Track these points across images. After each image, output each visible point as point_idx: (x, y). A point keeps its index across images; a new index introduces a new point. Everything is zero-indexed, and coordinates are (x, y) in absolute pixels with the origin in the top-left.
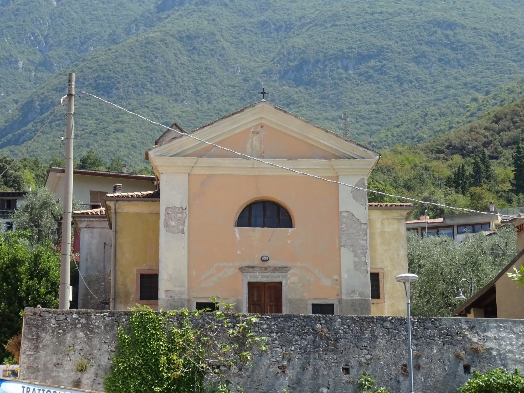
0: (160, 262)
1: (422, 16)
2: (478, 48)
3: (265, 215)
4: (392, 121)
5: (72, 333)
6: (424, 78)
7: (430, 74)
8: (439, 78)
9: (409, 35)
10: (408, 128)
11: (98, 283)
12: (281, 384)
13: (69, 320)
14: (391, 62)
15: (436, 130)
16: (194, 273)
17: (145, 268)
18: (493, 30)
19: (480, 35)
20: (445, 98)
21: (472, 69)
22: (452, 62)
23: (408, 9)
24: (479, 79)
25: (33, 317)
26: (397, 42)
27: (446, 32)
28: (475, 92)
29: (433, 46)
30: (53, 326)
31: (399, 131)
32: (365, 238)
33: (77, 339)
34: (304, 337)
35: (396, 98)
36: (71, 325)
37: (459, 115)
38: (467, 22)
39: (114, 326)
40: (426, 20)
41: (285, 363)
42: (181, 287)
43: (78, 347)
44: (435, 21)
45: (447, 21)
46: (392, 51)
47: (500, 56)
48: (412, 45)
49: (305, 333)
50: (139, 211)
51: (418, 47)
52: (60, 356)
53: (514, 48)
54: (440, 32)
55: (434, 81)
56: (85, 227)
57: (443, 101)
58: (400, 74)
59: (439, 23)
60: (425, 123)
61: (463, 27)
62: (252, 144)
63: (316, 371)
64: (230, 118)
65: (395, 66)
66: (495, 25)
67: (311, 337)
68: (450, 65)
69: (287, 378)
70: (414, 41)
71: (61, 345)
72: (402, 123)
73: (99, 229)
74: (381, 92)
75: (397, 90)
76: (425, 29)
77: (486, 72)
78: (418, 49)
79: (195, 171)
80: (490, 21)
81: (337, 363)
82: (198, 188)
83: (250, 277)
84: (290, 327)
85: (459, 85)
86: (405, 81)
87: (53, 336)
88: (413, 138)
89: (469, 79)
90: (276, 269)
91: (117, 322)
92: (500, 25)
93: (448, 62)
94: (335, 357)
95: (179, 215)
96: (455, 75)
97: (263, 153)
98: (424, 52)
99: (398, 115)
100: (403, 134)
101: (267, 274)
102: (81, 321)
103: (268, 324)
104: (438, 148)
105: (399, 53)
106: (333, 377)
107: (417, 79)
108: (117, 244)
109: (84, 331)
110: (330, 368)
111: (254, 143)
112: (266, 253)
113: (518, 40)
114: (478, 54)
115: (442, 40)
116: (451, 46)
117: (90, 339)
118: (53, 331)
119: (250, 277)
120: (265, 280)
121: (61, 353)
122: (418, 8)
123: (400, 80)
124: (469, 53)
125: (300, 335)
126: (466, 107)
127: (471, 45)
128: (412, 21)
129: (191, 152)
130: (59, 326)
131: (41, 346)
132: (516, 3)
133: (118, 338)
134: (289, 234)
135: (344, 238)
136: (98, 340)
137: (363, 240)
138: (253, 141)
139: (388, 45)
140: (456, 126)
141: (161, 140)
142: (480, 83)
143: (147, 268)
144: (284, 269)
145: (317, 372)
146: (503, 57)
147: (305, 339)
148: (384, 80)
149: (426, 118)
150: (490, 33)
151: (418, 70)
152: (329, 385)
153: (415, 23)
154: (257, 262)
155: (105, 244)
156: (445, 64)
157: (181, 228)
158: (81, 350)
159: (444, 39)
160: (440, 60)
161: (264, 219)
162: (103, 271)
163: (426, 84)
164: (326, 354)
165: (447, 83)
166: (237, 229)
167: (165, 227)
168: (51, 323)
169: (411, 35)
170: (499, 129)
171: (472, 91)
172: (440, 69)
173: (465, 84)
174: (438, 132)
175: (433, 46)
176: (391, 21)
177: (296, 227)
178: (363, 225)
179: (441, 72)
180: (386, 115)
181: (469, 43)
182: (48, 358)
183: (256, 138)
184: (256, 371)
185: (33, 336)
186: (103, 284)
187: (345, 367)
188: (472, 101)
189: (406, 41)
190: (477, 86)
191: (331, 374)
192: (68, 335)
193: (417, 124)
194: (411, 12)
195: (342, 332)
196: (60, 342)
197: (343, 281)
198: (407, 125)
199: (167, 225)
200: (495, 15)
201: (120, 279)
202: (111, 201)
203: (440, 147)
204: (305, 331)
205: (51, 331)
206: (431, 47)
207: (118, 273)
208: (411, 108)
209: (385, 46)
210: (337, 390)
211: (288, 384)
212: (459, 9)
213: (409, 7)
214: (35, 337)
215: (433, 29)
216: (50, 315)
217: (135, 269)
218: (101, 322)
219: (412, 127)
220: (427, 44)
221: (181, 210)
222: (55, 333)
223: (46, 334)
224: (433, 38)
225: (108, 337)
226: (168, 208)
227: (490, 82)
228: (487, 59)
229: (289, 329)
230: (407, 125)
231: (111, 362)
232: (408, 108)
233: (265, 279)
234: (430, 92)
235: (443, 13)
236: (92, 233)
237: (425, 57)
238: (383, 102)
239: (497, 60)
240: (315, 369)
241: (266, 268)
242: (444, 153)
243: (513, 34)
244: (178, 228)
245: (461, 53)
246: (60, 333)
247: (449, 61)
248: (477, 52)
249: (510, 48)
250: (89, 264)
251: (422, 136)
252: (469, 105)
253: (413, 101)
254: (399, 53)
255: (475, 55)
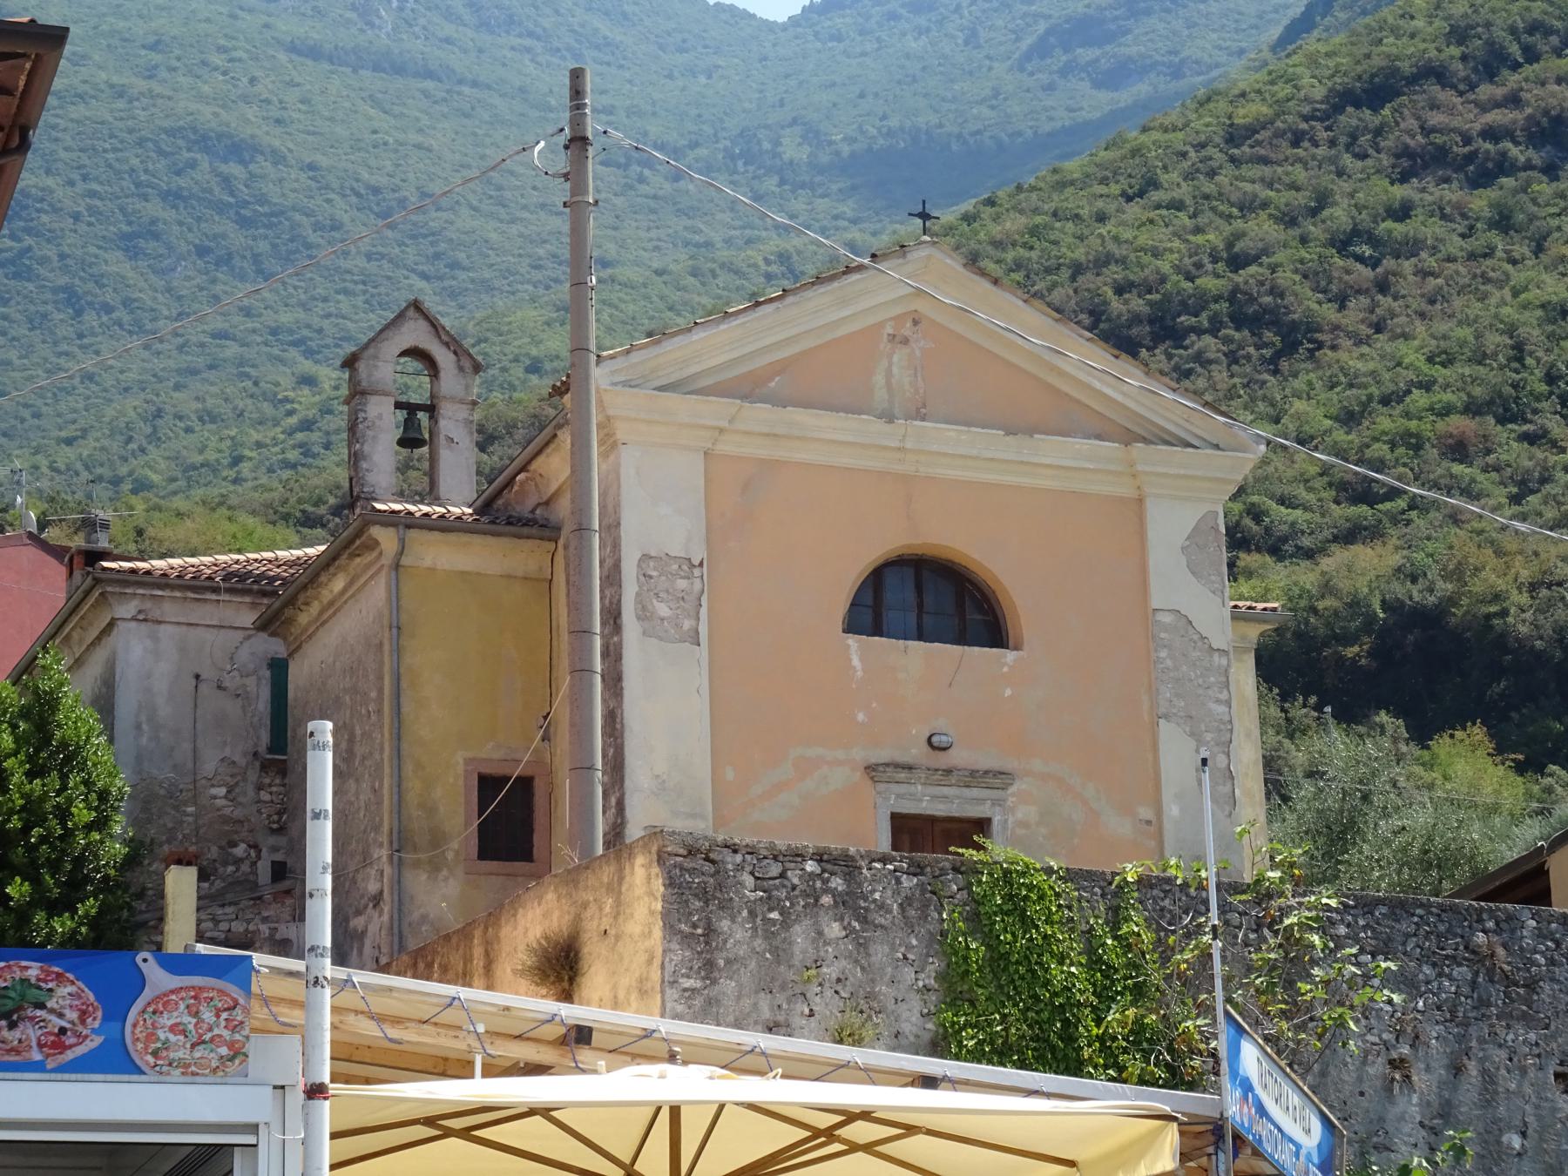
0: (627, 734)
1: (153, 110)
2: (317, 227)
3: (920, 606)
4: (43, 422)
5: (807, 922)
6: (149, 303)
7: (169, 290)
8: (196, 306)
9: (110, 166)
10: (103, 449)
11: (176, 808)
12: (1402, 1118)
13: (796, 881)
14: (48, 241)
15: (189, 461)
16: (730, 774)
17: (508, 751)
18: (365, 175)
19: (327, 187)
20: (211, 367)
21: (295, 288)
22: (237, 262)
23: (112, 86)
24: (316, 320)
25: (688, 864)
26: (71, 183)
27: (223, 168)
28: (301, 359)
29: (182, 205)
30: (752, 896)
31: (73, 457)
32: (1224, 696)
33: (826, 943)
34: (1446, 970)
35: (60, 354)
36: (805, 895)
37: (260, 423)
38: (291, 146)
39: (928, 906)
40: (166, 124)
41: (1405, 1050)
42: (693, 816)
43: (830, 971)
44: (195, 130)
45: (231, 136)
46: (56, 210)
47: (383, 256)
48: (118, 198)
49: (1447, 957)
50: (461, 567)
51: (138, 206)
52: (781, 998)
53: (425, 236)
54: (206, 165)
55: (180, 314)
56: (134, 619)
57: (205, 375)
58: (77, 281)
59: (205, 138)
60: (154, 437)
61: (278, 158)
62: (889, 374)
63: (1488, 1078)
64: (836, 284)
65: (62, 256)
66: (373, 162)
67: (1461, 972)
68: (232, 269)
69: (1415, 1099)
70: (124, 183)
71: (779, 963)
72: (85, 432)
73: (177, 629)
74: (13, 333)
75: (61, 332)
76: (161, 152)
77: (338, 302)
78: (134, 212)
79: (727, 446)
80: (359, 150)
81: (1539, 1056)
82: (738, 496)
83: (898, 796)
84: (1408, 936)
85: (254, 331)
86: (90, 304)
87: (754, 929)
88: (116, 482)
89: (286, 318)
90: (976, 777)
91: (933, 893)
92: (388, 163)
93: (226, 260)
94: (1532, 1036)
95: (682, 584)
96: (246, 302)
97: (924, 406)
98: (154, 222)
99: (62, 407)
100: (87, 468)
101: (946, 790)
102: (832, 885)
103: (1348, 926)
104: (303, 511)
105: (76, 217)
106: (1534, 1099)
107: (127, 302)
108: (402, 671)
109: (842, 919)
110: (1523, 1071)
111: (895, 370)
112: (940, 724)
113: (439, 214)
114: (318, 246)
115: (210, 191)
116: (237, 213)
117: (862, 945)
118: (752, 914)
119: (898, 796)
120: (940, 810)
121: (783, 988)
122: (142, 84)
123: (73, 301)
124: (292, 240)
125: (1434, 965)
126: (281, 401)
127: (297, 217)
128: (120, 124)
129: (709, 381)
130: (769, 898)
131: (721, 963)
132: (435, 102)
133: (941, 941)
134: (1005, 669)
135: (1166, 693)
136: (886, 949)
137: (1218, 701)
138: (890, 365)
139: (43, 190)
140: (253, 454)
141: (371, 351)
142: (320, 331)
143: (497, 755)
144: (997, 778)
145: (1493, 1082)
146: (391, 261)
147: (1450, 978)
148: (26, 297)
149: (159, 422)
150: (355, 185)
151: (131, 274)
152: (1525, 1124)
153: (131, 131)
154: (916, 752)
155: (197, 677)
156: (217, 264)
157: (687, 624)
158: (839, 980)
159: (217, 190)
160: (202, 251)
161: (919, 616)
162: (190, 765)
163: (154, 320)
164: (1508, 1027)
165: (219, 324)
166: (853, 641)
167: (638, 618)
168: (741, 884)
169: (117, 165)
170: (492, 469)
171: (293, 353)
172: (200, 280)
173: (274, 332)
174: (195, 468)
175: (182, 205)
176: (57, 116)
177: (1026, 646)
178: (1216, 656)
179: (201, 289)
180: (26, 406)
181: (294, 209)
182: (747, 1003)
183: (899, 356)
184: (1333, 1072)
185: (695, 926)
186: (190, 809)
187: (1560, 1069)
188: (299, 383)
189: (101, 183)
190: (311, 339)
191: (1528, 1090)
192: (797, 928)
193: (130, 439)
194: (121, 95)
195: (1543, 961)
196: (775, 951)
197: (1168, 826)
198: (97, 440)
199: (644, 614)
200: (375, 132)
201: (414, 786)
202: (385, 524)
203: (310, 509)
204: (1449, 952)
205: (745, 913)
206: (174, 207)
207: (408, 768)
208: (105, 390)
209: (34, 191)
210: (1546, 1141)
211: (1418, 1119)
212: (268, 101)
213: (115, 79)
214: (700, 931)
215: (187, 155)
216: (739, 858)
217: (459, 758)
218: (889, 893)
219: (115, 446)
220: (164, 199)
221: (685, 567)
222: (758, 920)
223: (733, 920)
224: (182, 182)
225: (914, 942)
226: (646, 557)
227: (349, 331)
228: (341, 263)
229: (1404, 944)
230: (97, 440)
231: (930, 1026)
232: (94, 387)
233: (941, 806)
234: (166, 346)
235: (217, 110)
236: (155, 639)
237: (156, 236)
238: (17, 362)
239: (372, 267)
240: (1484, 1072)
241: (948, 772)
242: (323, 526)
243: (424, 195)
244: (678, 626)
245: (266, 237)
246: (774, 922)
247: (230, 256)
248: (313, 238)
249: (414, 237)
250: (144, 740)
251: (147, 478)
252: (291, 394)
253: (111, 367)
254: (76, 217)
255: (309, 246)
